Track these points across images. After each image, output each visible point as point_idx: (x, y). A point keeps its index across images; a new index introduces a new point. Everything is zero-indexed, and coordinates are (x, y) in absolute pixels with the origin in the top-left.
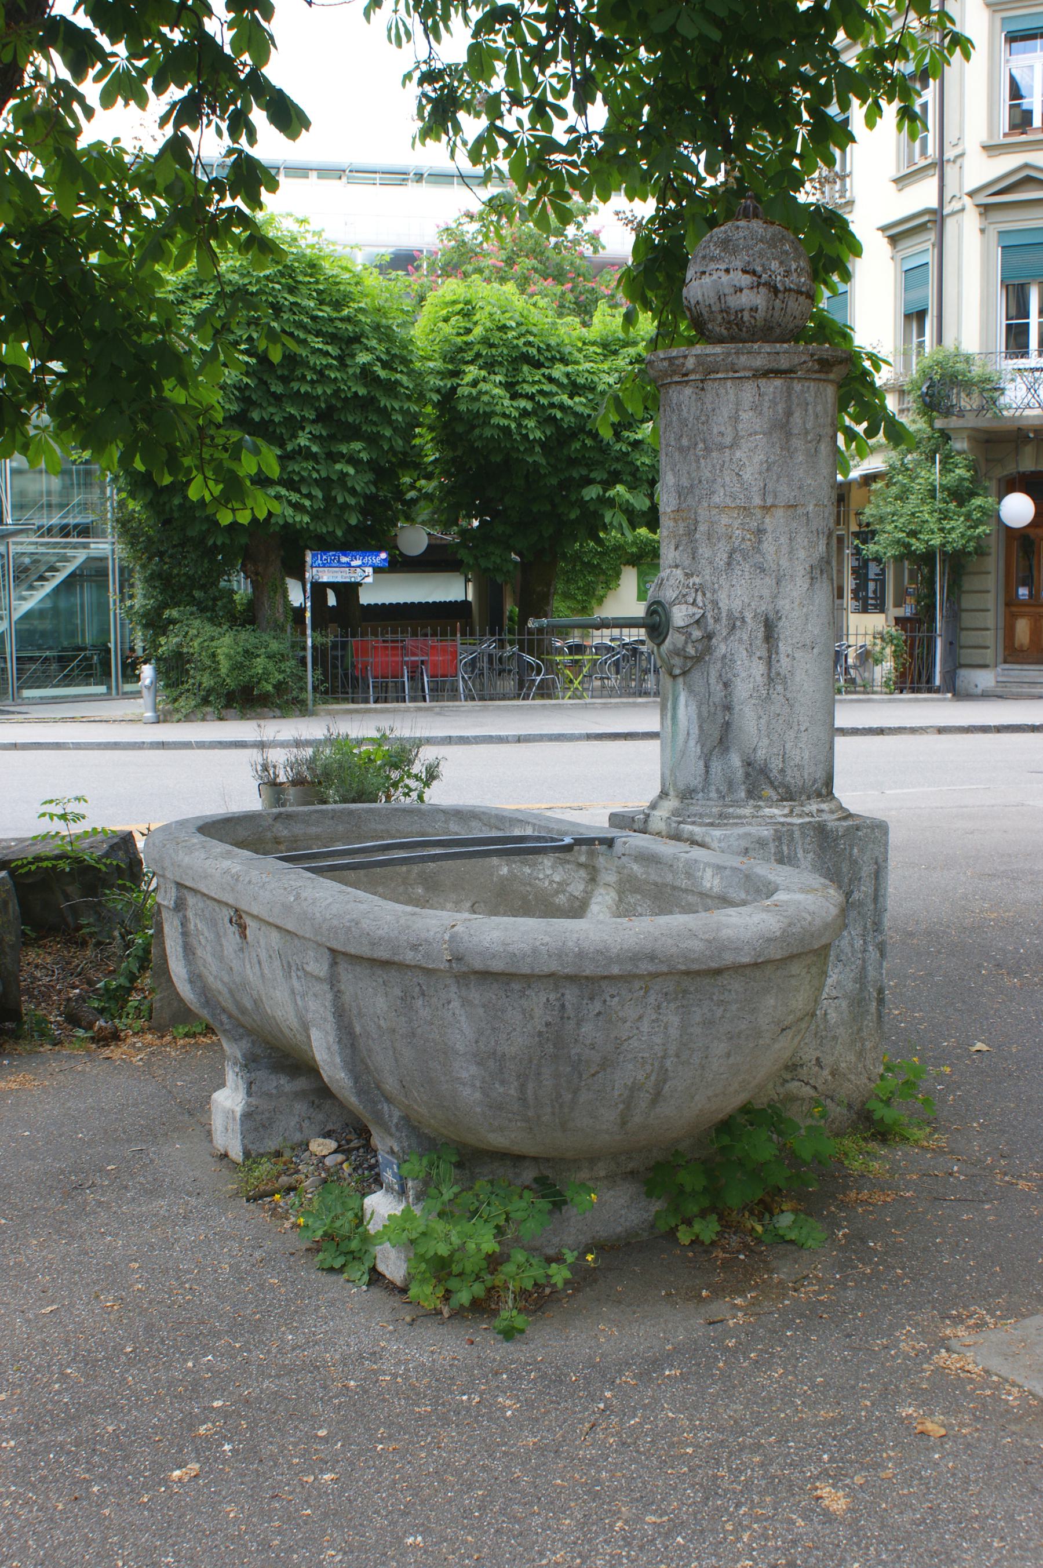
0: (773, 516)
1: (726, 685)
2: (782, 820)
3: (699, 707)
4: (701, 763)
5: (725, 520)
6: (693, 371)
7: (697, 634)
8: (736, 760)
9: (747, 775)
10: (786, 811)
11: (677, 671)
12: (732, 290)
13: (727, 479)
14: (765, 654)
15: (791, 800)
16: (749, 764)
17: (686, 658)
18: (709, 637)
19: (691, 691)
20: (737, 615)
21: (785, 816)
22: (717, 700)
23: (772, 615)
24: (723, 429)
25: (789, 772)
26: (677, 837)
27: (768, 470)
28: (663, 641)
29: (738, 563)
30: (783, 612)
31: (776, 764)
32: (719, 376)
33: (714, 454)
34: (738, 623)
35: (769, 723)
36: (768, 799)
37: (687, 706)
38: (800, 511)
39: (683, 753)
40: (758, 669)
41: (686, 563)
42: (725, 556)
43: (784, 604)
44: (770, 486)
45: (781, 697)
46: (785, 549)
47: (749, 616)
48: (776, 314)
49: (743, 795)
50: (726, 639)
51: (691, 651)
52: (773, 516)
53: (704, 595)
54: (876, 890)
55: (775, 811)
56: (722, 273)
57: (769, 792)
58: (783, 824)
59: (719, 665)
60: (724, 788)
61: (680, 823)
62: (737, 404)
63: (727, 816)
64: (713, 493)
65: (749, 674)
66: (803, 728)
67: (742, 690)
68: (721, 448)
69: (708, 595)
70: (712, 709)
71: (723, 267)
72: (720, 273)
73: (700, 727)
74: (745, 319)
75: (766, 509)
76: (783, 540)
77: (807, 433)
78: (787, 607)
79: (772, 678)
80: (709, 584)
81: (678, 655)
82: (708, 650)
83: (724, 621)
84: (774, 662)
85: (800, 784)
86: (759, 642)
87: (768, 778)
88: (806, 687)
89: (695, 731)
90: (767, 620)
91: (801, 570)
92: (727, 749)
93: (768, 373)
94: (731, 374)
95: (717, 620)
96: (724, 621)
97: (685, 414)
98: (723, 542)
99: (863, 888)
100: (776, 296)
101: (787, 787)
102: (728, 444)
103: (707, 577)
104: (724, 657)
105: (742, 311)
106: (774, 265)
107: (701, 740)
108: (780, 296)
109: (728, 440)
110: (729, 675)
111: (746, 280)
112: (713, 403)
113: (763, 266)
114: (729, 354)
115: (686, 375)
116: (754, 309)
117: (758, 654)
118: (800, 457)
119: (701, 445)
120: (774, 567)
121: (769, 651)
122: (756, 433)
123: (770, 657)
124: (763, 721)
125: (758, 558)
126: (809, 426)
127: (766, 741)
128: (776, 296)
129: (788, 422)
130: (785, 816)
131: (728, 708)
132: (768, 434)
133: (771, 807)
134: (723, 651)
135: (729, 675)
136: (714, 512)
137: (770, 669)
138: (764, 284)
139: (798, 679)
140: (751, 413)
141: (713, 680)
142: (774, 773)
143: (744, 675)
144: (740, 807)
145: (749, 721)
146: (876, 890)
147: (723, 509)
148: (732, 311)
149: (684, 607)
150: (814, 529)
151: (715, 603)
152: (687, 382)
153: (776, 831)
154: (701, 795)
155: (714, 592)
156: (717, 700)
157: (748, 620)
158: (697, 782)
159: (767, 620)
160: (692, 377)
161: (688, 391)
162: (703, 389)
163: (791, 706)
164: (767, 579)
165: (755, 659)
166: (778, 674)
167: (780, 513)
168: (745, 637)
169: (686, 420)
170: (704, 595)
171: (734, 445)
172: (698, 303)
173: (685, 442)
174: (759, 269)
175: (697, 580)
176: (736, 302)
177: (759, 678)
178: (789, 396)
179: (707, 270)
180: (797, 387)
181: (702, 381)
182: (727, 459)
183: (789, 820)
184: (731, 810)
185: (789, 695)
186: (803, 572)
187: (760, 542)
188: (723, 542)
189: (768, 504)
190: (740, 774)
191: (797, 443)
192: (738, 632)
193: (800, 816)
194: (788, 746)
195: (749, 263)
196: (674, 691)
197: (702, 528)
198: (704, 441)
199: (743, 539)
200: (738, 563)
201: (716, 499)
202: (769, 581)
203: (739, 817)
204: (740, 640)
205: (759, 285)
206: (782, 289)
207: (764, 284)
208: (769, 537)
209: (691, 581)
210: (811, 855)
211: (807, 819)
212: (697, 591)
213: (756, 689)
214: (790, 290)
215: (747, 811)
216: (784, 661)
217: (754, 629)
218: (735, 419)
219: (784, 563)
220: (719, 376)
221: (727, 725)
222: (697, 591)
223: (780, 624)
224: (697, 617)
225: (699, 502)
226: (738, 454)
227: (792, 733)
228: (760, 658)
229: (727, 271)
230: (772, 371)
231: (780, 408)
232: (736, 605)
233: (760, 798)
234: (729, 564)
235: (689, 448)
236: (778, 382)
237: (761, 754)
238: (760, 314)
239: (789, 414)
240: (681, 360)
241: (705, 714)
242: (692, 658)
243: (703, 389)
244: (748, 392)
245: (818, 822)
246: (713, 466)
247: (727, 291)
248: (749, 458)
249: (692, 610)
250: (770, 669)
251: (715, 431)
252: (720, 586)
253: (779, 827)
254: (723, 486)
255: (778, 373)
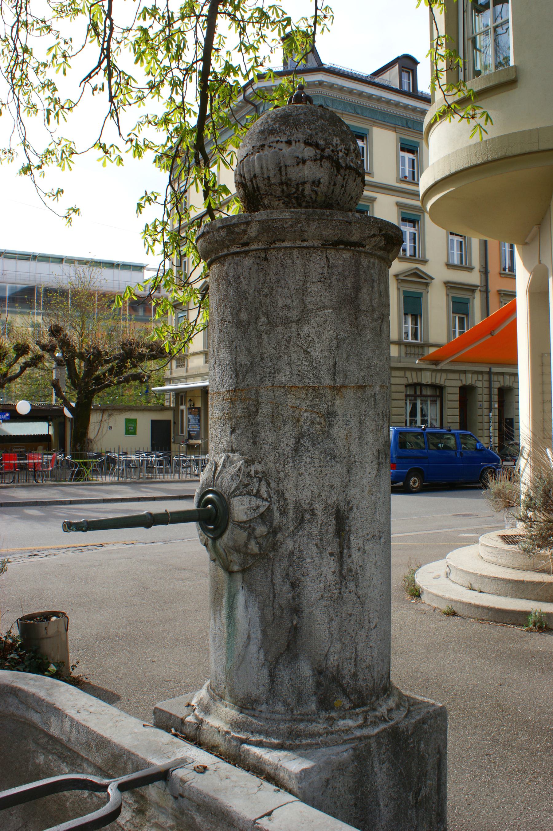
0: (261, 396)
1: (294, 585)
2: (358, 733)
3: (262, 609)
4: (265, 672)
5: (291, 401)
6: (256, 239)
7: (261, 530)
8: (305, 669)
9: (319, 685)
10: (360, 721)
11: (236, 568)
12: (294, 161)
13: (294, 356)
14: (336, 550)
15: (363, 704)
16: (320, 673)
17: (246, 554)
18: (274, 532)
19: (251, 589)
20: (306, 507)
21: (360, 727)
22: (283, 602)
23: (343, 506)
24: (289, 302)
25: (361, 676)
26: (236, 759)
27: (338, 347)
28: (221, 535)
29: (307, 449)
30: (355, 502)
31: (348, 669)
32: (285, 244)
33: (279, 329)
34: (307, 516)
35: (341, 626)
36: (342, 708)
37: (246, 607)
38: (369, 392)
39: (243, 658)
40: (329, 567)
41: (246, 448)
42: (292, 441)
43: (354, 493)
44: (340, 365)
45: (353, 596)
46: (355, 434)
47: (319, 508)
48: (337, 190)
49: (314, 707)
50: (293, 534)
51: (254, 548)
52: (343, 397)
53: (268, 484)
54: (439, 780)
55: (350, 723)
56: (283, 146)
57: (342, 701)
58: (360, 739)
59: (286, 563)
60: (292, 700)
61: (243, 741)
62: (306, 275)
63: (299, 735)
64: (279, 371)
65: (319, 571)
66: (372, 625)
67: (312, 590)
68: (287, 322)
69: (273, 484)
70: (278, 613)
71: (284, 139)
72: (280, 146)
73: (264, 632)
74: (306, 192)
75: (337, 389)
76: (354, 423)
77: (373, 311)
78: (358, 497)
79: (345, 574)
80: (273, 472)
81: (238, 551)
82: (275, 547)
83: (291, 514)
84: (345, 558)
85: (370, 685)
86: (330, 537)
87: (341, 685)
88: (375, 581)
89: (257, 635)
90: (338, 511)
91: (369, 456)
92: (295, 658)
93: (337, 244)
94: (298, 243)
95: (283, 513)
96: (291, 514)
97: (244, 286)
98: (289, 425)
99: (429, 782)
100: (338, 171)
101: (359, 693)
102: (295, 318)
103: (271, 465)
104: (291, 554)
105: (304, 183)
106: (336, 140)
107: (264, 646)
108: (342, 171)
109: (294, 314)
110: (298, 574)
111: (309, 152)
112: (277, 274)
113: (325, 140)
114: (298, 221)
115: (246, 244)
116: (317, 183)
117: (329, 550)
118: (368, 336)
119: (263, 319)
120: (345, 453)
121: (341, 546)
122: (325, 307)
123: (341, 553)
124: (334, 624)
125: (329, 444)
126: (375, 303)
127: (338, 646)
128: (338, 171)
129: (356, 296)
130: (360, 727)
131: (296, 610)
132: (337, 309)
133: (344, 718)
134: (290, 547)
135: (298, 574)
136: (279, 392)
137: (341, 566)
138: (329, 158)
139: (368, 574)
140: (320, 286)
141: (278, 580)
142: (347, 680)
143: (313, 573)
144: (311, 721)
145: (320, 624)
146: (439, 780)
147: (289, 389)
148: (294, 183)
149: (246, 499)
150: (380, 412)
151: (281, 494)
152: (246, 253)
153: (354, 749)
154: (264, 707)
155: (280, 480)
156: (283, 602)
157: (319, 513)
158: (260, 691)
159: (338, 511)
160: (254, 246)
161: (248, 262)
162: (266, 259)
163: (362, 604)
164: (338, 466)
165: (326, 556)
166: (350, 570)
167: (350, 394)
168: (315, 531)
169: (245, 292)
170: (268, 484)
171: (302, 320)
172: (255, 176)
173: (244, 316)
174: (322, 143)
175: (259, 468)
176: (296, 174)
177: (330, 577)
178: (358, 270)
179: (267, 143)
180: (365, 262)
181: (265, 250)
182: (294, 334)
183: (365, 732)
184: (302, 726)
185: (360, 592)
186: (371, 458)
187: (330, 426)
188: (289, 425)
189: (339, 384)
190: (310, 684)
191: (364, 320)
192: (307, 527)
193: (374, 724)
194: (359, 648)
195: (311, 135)
196: (229, 592)
197: (265, 410)
198: (267, 314)
199: (312, 422)
200: (307, 449)
201: (282, 378)
202: (339, 468)
203: (312, 735)
204: (310, 535)
205: (322, 157)
206: (344, 165)
207: (329, 158)
208: (339, 421)
209: (253, 469)
210: (386, 765)
211: (382, 726)
212: (260, 480)
213: (327, 589)
214: (350, 168)
215: (319, 727)
216: (356, 555)
217: (324, 520)
218: (304, 291)
219: (355, 448)
220: (285, 244)
221: (295, 630)
222: (260, 480)
223: (352, 515)
224: (262, 510)
225: (261, 381)
226: (306, 329)
227: (363, 633)
228: (331, 554)
229: (289, 143)
230: (341, 242)
231: (349, 282)
232: (305, 496)
233: (333, 708)
234: (296, 450)
235: (249, 322)
236: (347, 255)
237: (333, 659)
238: (322, 189)
239: (357, 289)
240: (243, 227)
241: (270, 617)
242: (254, 556)
243: (266, 259)
244: (316, 265)
245: (392, 727)
246: (278, 342)
247: (288, 163)
248: (319, 334)
249: (255, 502)
250: (341, 566)
251: (280, 304)
252: (286, 475)
253: (357, 743)
254: (290, 364)
255: (349, 245)
